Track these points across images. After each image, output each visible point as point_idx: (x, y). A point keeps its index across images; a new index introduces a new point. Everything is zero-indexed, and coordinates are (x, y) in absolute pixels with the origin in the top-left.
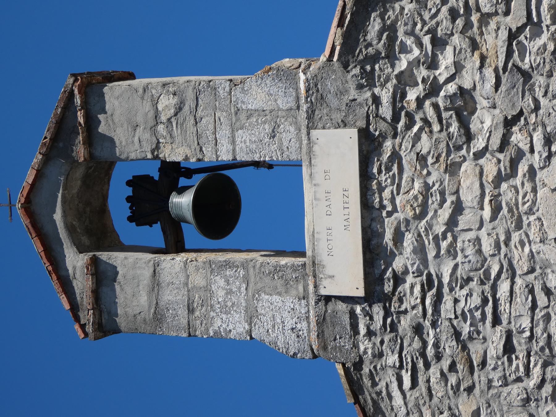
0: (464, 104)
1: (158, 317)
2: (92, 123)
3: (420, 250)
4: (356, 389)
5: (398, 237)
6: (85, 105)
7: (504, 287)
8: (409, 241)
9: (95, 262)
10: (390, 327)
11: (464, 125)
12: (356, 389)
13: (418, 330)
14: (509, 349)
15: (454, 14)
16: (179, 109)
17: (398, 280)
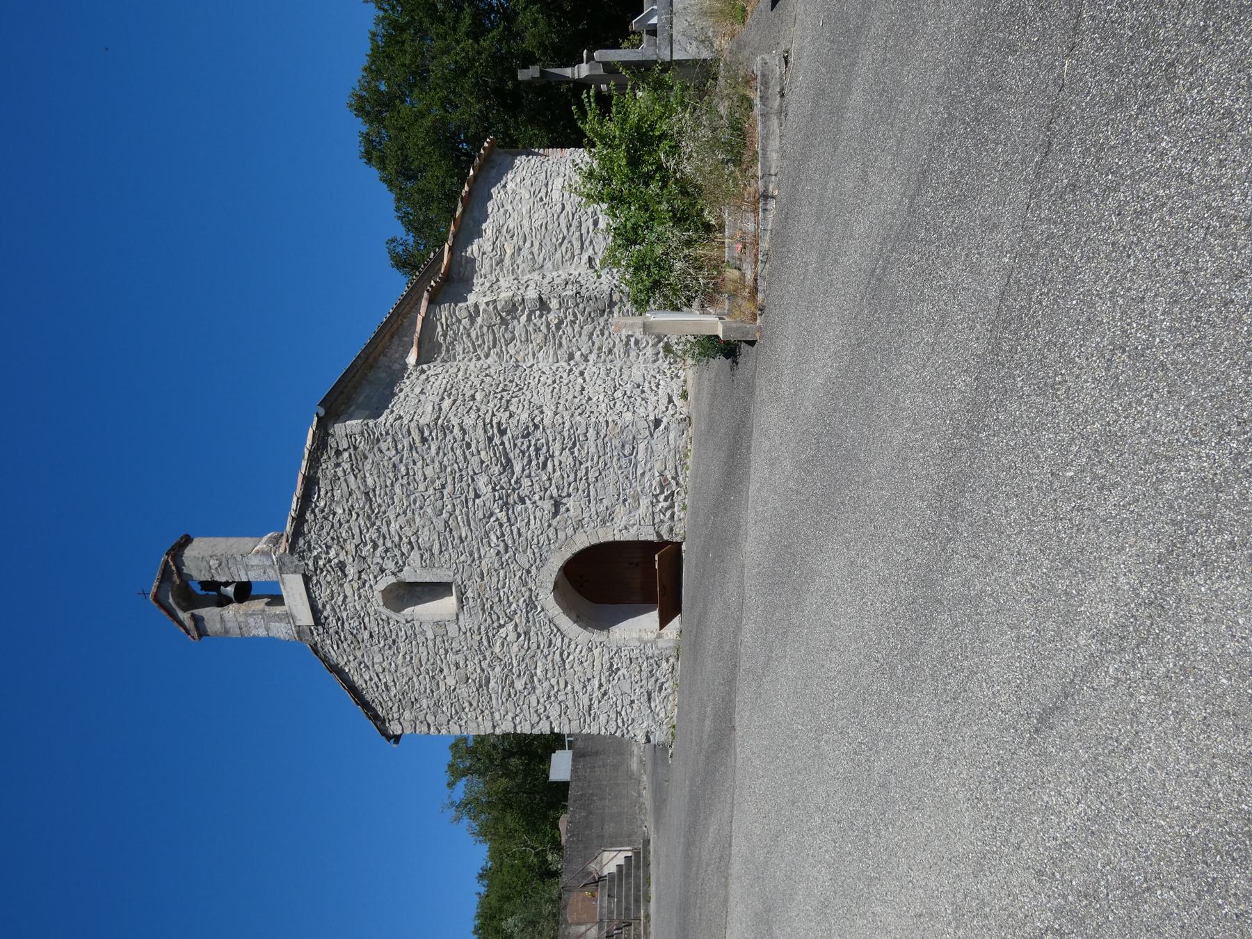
0: (342, 566)
1: (226, 631)
2: (179, 571)
3: (333, 609)
4: (316, 652)
5: (324, 606)
6: (175, 564)
7: (366, 619)
8: (328, 607)
9: (193, 615)
10: (454, 237)
11: (343, 572)
12: (316, 652)
13: (337, 633)
14: (371, 636)
15: (333, 539)
16: (220, 565)
17: (326, 618)
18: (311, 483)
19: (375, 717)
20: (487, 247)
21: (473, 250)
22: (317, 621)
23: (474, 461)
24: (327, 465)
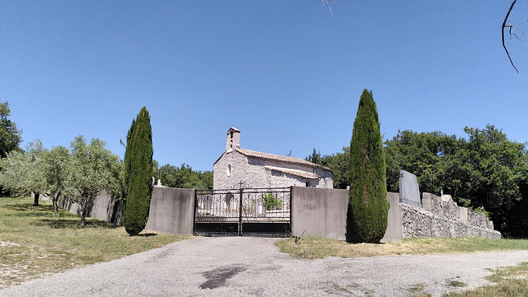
18: (241, 153)
21: (285, 176)
24: (243, 156)
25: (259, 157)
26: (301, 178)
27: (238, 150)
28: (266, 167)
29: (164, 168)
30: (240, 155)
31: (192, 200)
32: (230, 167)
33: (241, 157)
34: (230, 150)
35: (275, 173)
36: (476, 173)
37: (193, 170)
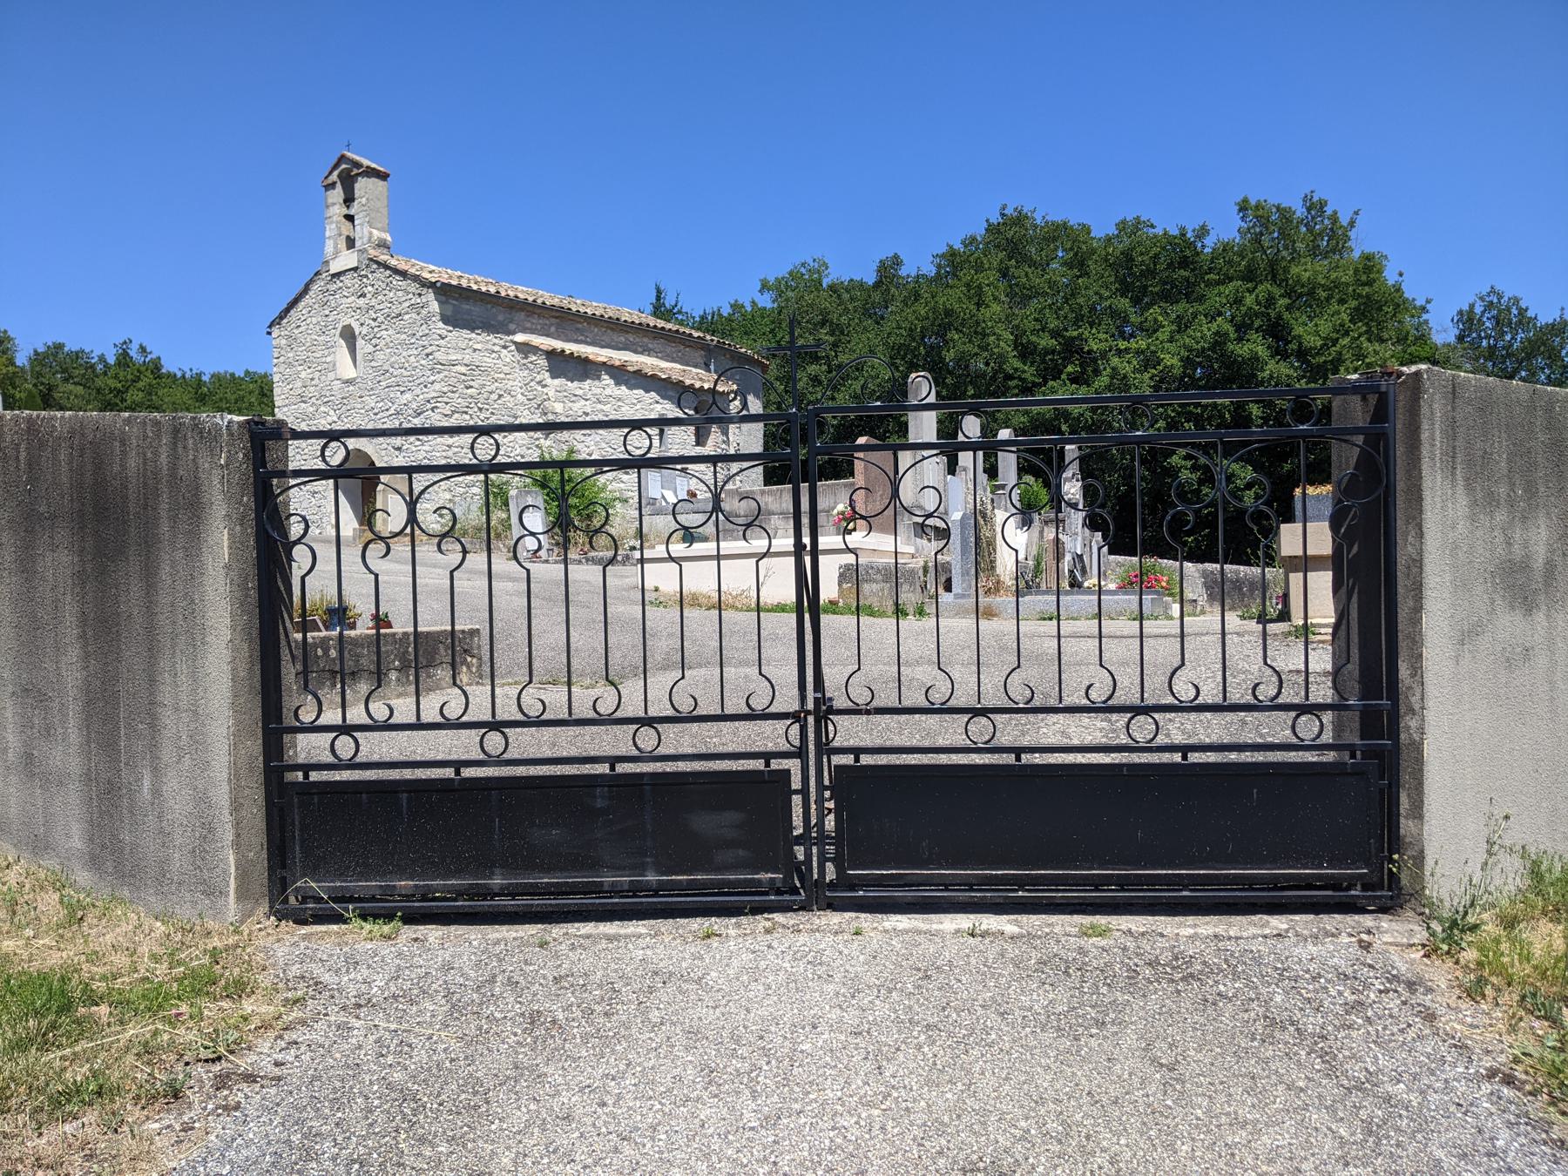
0: (363, 295)
18: (404, 274)
19: (281, 317)
20: (608, 391)
21: (607, 380)
22: (333, 276)
23: (418, 391)
24: (413, 287)
25: (487, 294)
26: (674, 390)
27: (383, 258)
28: (520, 338)
29: (38, 359)
30: (397, 281)
31: (222, 543)
32: (349, 336)
33: (401, 295)
34: (348, 260)
35: (561, 364)
36: (1276, 369)
37: (169, 366)
